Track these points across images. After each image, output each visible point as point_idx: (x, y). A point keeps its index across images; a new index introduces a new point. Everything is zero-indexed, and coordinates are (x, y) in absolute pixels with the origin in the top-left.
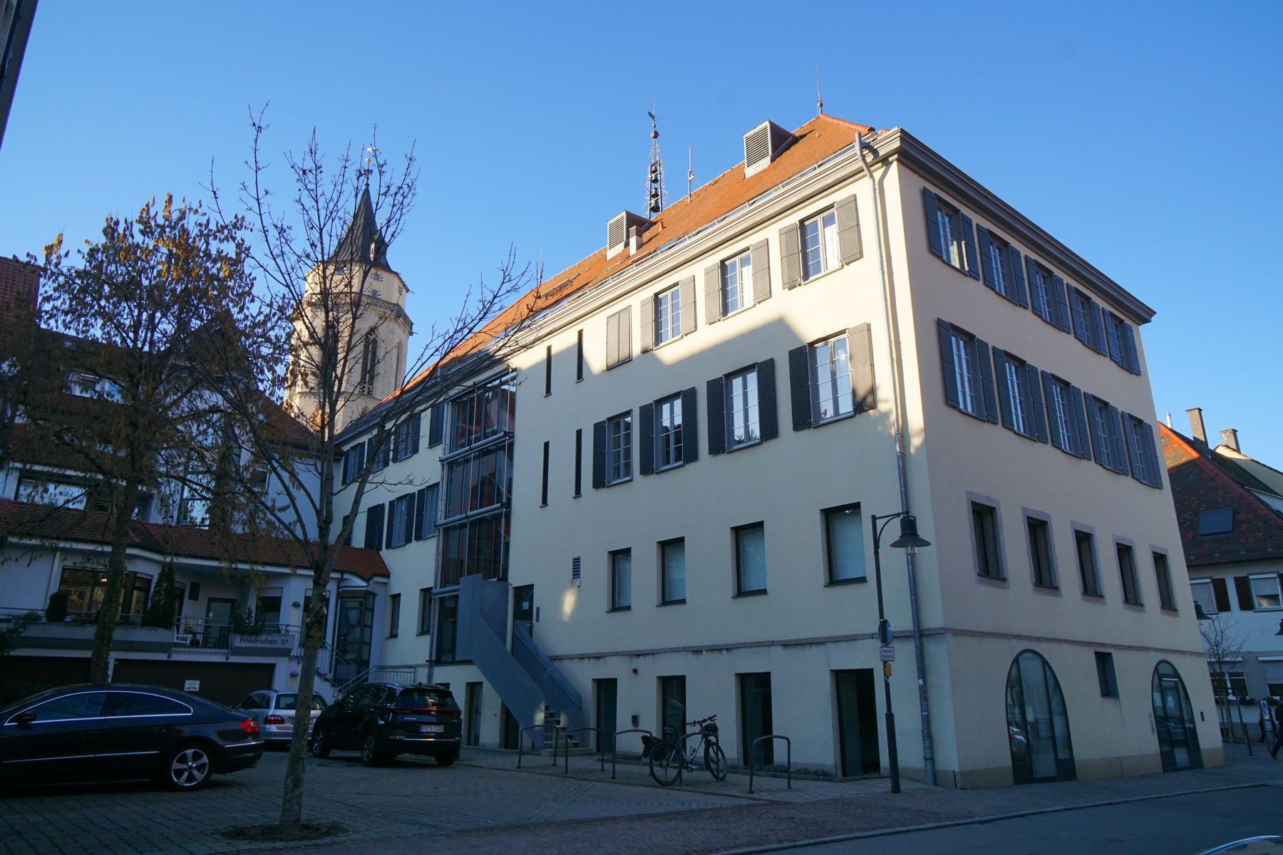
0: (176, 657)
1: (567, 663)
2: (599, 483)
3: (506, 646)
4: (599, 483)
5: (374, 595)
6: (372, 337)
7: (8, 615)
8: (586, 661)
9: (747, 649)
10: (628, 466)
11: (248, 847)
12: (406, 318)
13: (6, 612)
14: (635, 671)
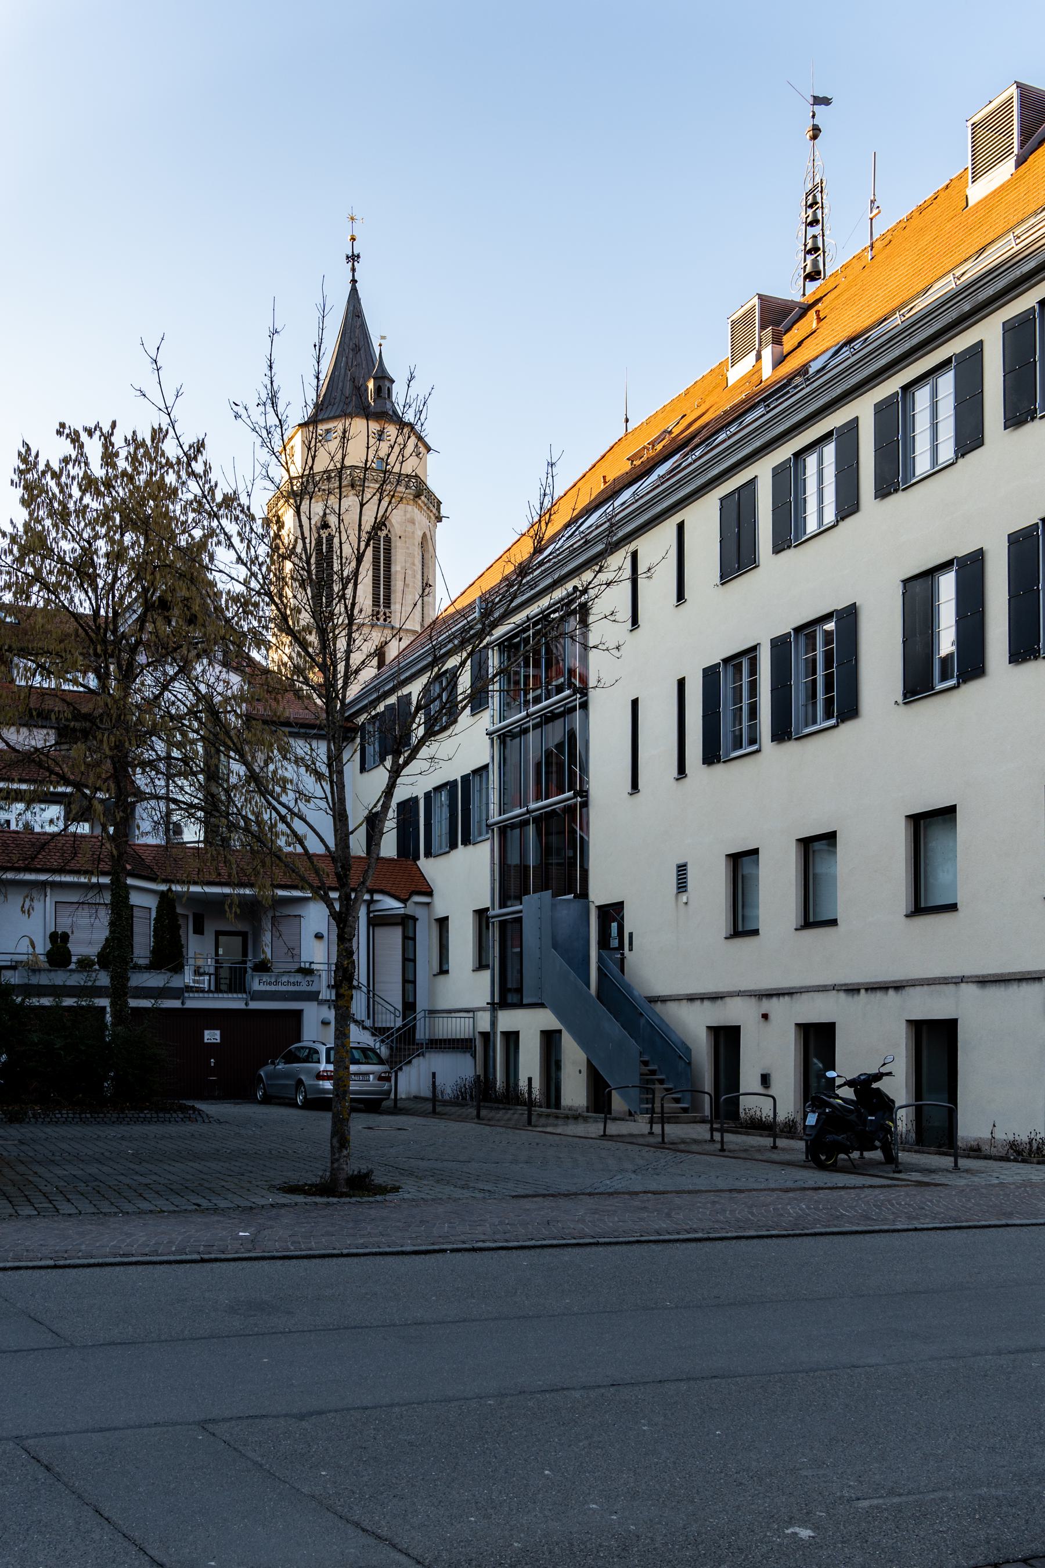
0: (190, 1004)
1: (672, 1006)
2: (711, 756)
4: (711, 756)
5: (415, 919)
7: (11, 961)
10: (754, 729)
11: (305, 1200)
12: (430, 495)
13: (8, 957)
14: (765, 1016)
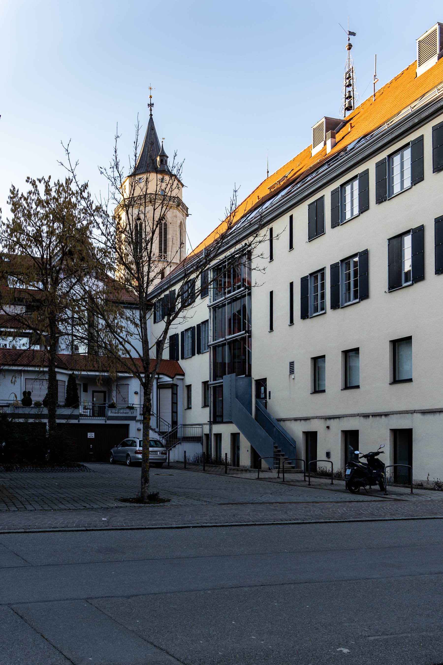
0: (82, 422)
1: (288, 423)
2: (305, 315)
3: (252, 415)
4: (305, 315)
5: (177, 386)
6: (163, 222)
7: (7, 403)
8: (299, 421)
9: (398, 415)
10: (323, 304)
11: (130, 505)
12: (183, 205)
14: (328, 427)
